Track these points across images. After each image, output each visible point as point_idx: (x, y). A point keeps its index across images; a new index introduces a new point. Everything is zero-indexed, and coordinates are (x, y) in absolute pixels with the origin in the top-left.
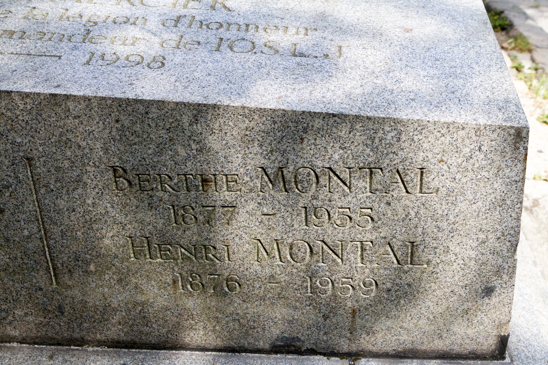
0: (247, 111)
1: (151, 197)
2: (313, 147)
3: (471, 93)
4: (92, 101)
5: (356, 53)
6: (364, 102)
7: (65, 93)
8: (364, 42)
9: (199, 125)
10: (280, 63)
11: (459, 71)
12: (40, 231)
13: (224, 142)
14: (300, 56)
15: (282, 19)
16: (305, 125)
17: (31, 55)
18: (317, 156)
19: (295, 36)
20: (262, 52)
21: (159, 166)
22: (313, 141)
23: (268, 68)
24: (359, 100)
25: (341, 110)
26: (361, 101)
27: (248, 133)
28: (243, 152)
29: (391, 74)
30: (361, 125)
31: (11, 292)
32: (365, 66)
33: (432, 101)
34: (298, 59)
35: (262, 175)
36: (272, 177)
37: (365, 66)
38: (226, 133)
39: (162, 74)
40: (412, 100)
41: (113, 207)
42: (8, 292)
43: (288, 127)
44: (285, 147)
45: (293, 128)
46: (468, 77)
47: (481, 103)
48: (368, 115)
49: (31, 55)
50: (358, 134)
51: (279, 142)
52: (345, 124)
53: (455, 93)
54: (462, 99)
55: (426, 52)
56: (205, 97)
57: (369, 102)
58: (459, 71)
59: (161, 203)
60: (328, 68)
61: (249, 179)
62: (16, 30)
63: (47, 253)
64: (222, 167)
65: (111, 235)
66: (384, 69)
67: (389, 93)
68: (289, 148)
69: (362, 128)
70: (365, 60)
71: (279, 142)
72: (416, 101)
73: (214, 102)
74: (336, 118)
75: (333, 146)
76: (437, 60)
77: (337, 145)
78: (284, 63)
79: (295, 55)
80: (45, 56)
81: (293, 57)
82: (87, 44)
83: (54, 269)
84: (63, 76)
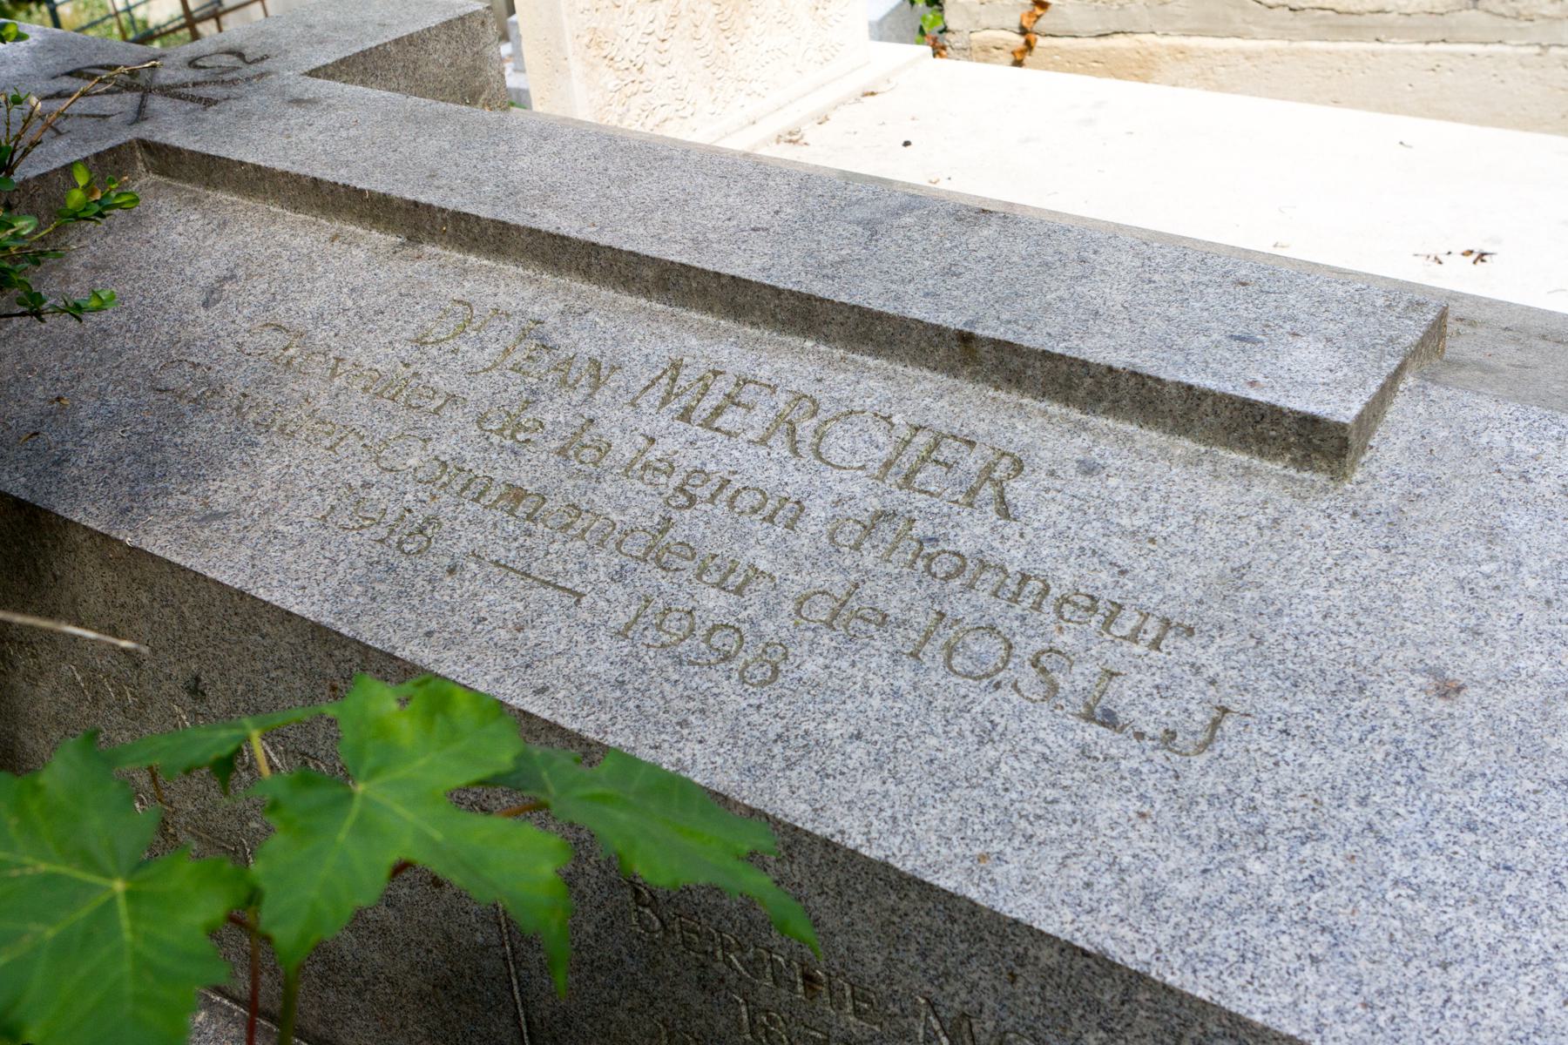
0: (893, 877)
1: (703, 966)
2: (1038, 1000)
3: (1499, 982)
4: (594, 748)
5: (1253, 747)
6: (1181, 933)
7: (546, 715)
8: (1296, 709)
9: (795, 867)
10: (1042, 735)
11: (1510, 889)
12: (503, 945)
13: (846, 919)
14: (1103, 724)
15: (1123, 572)
16: (1020, 950)
17: (529, 576)
18: (1047, 1022)
19: (1126, 643)
20: (1015, 686)
21: (719, 916)
22: (1037, 989)
23: (1002, 747)
24: (1173, 920)
25: (1110, 945)
26: (1177, 925)
27: (896, 919)
28: (885, 953)
29: (1306, 851)
30: (1148, 996)
31: (454, 1031)
32: (1252, 799)
33: (1366, 978)
34: (1092, 732)
35: (927, 1015)
36: (948, 1026)
37: (1252, 799)
38: (850, 903)
39: (759, 707)
40: (1314, 960)
41: (632, 957)
42: (449, 1027)
43: (982, 939)
44: (975, 976)
45: (992, 946)
46: (1526, 915)
47: (1506, 1028)
48: (1169, 979)
49: (529, 576)
50: (1142, 1013)
51: (962, 963)
52: (1109, 981)
53: (1451, 969)
54: (1456, 998)
55: (1455, 786)
56: (815, 810)
57: (1194, 935)
58: (1510, 889)
59: (722, 987)
60: (1150, 783)
61: (897, 1010)
62: (531, 489)
63: (516, 989)
64: (843, 965)
65: (628, 1005)
66: (1297, 822)
67: (1265, 918)
68: (982, 983)
69: (1151, 1004)
70: (1264, 776)
71: (962, 963)
72: (1323, 967)
73: (828, 831)
74: (1090, 962)
75: (1083, 1016)
76: (1471, 827)
77: (1094, 1019)
78: (1050, 739)
79: (1089, 717)
80: (556, 586)
81: (1082, 723)
82: (648, 567)
83: (528, 1023)
84: (562, 661)
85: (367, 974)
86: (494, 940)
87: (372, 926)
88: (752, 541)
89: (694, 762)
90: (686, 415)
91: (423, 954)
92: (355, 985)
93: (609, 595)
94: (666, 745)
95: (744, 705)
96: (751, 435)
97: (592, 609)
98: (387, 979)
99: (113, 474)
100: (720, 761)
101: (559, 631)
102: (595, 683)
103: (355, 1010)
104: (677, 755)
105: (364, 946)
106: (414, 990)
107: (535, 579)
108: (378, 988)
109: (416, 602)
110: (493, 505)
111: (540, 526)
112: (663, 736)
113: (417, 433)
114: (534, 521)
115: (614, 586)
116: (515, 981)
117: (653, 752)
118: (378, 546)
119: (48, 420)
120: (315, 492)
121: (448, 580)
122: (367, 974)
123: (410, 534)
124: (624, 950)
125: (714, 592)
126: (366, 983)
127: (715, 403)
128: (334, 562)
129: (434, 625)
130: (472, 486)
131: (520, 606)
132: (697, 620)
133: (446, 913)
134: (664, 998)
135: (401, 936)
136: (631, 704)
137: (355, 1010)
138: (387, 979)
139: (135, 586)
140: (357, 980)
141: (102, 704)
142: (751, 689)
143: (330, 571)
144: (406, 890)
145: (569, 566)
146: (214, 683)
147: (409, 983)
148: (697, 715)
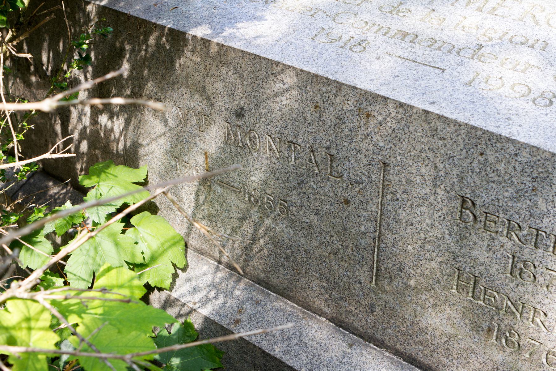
1: (493, 239)
7: (437, 112)
12: (375, 232)
17: (416, 62)
39: (547, 114)
41: (450, 235)
59: (502, 249)
63: (376, 253)
80: (430, 66)
82: (474, 61)
83: (377, 270)
84: (441, 93)
85: (294, 248)
86: (371, 229)
87: (304, 225)
88: (525, 54)
89: (518, 134)
90: (480, 10)
91: (328, 237)
92: (286, 254)
93: (458, 70)
94: (502, 126)
95: (539, 113)
96: (513, 17)
97: (451, 75)
98: (305, 250)
99: (212, 21)
100: (532, 134)
101: (436, 82)
102: (459, 102)
103: (283, 266)
104: (509, 130)
105: (296, 235)
106: (318, 255)
107: (419, 63)
108: (298, 255)
109: (363, 68)
110: (393, 37)
111: (418, 45)
112: (499, 123)
113: (351, 12)
114: (414, 43)
115: (459, 67)
116: (376, 250)
117: (496, 128)
118: (341, 49)
119: (182, 3)
120: (307, 29)
121: (377, 62)
122: (294, 248)
123: (355, 45)
124: (447, 232)
125: (511, 71)
126: (292, 253)
127: (493, 6)
128: (320, 53)
129: (373, 77)
130: (381, 30)
131: (415, 72)
132: (505, 81)
133: (347, 217)
134: (463, 256)
135: (319, 229)
136: (480, 110)
137: (283, 266)
138: (305, 250)
139: (221, 65)
140: (288, 251)
141: (189, 125)
142: (540, 108)
143: (319, 56)
144: (328, 207)
145: (435, 59)
146: (250, 110)
147: (316, 253)
148: (515, 115)
